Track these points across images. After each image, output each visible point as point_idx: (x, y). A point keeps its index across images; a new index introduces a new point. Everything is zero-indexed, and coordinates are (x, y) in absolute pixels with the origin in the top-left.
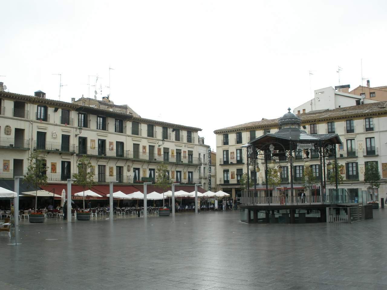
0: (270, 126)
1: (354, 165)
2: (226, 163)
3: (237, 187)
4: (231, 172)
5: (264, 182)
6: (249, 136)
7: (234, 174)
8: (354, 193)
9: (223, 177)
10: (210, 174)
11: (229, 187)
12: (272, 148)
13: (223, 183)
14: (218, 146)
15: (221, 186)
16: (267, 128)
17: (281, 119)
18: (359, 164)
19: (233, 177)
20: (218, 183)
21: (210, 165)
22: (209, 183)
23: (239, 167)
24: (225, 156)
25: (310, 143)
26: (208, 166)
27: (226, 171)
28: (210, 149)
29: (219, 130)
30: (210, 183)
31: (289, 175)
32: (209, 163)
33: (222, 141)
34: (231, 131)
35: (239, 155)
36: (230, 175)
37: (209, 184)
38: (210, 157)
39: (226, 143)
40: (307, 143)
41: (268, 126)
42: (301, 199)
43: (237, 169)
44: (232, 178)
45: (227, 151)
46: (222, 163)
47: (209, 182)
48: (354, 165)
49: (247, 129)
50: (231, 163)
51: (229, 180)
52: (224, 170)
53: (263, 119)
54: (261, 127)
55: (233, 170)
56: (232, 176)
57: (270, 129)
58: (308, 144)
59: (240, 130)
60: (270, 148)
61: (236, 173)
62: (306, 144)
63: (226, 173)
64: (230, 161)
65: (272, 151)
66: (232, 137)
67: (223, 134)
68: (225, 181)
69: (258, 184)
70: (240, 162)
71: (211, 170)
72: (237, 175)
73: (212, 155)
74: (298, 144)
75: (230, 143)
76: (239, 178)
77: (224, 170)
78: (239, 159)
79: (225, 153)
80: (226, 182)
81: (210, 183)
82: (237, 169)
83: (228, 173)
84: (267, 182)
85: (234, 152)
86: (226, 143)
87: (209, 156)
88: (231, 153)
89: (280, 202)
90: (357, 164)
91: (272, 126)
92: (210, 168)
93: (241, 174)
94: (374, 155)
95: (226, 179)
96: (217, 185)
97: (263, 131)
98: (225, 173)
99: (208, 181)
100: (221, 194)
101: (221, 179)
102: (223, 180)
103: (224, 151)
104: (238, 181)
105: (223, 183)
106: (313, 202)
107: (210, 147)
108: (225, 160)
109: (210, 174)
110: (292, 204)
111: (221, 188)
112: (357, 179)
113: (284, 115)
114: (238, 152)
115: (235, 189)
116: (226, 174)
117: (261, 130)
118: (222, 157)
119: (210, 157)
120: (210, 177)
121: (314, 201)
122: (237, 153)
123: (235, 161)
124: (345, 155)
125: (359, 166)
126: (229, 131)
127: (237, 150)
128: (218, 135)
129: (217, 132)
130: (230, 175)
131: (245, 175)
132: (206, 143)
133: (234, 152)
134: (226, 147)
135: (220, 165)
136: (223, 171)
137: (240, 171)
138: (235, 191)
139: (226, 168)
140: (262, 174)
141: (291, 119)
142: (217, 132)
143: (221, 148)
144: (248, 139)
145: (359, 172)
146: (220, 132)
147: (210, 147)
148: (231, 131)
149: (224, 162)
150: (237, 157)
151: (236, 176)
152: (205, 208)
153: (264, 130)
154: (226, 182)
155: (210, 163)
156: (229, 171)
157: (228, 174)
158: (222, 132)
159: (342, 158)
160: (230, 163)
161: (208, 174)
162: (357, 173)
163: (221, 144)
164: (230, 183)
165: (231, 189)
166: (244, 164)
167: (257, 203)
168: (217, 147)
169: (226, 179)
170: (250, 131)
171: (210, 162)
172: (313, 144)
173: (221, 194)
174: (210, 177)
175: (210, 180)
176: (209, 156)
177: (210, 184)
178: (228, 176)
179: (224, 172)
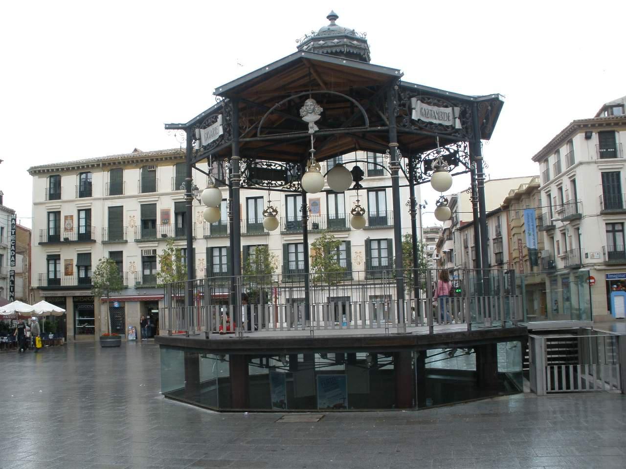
0: (157, 160)
1: (343, 247)
2: (54, 240)
3: (78, 293)
4: (65, 260)
5: (140, 282)
6: (109, 181)
7: (72, 265)
8: (340, 306)
9: (45, 271)
10: (13, 268)
11: (60, 293)
12: (313, 111)
13: (45, 284)
14: (38, 201)
15: (41, 292)
16: (151, 164)
17: (313, 39)
18: (352, 244)
19: (70, 270)
20: (35, 284)
21: (15, 251)
22: (10, 289)
23: (84, 249)
24: (52, 225)
25: (446, 107)
26: (9, 251)
27: (54, 259)
28: (14, 217)
29: (41, 167)
30: (14, 289)
31: (550, 168)
32: (12, 246)
33: (46, 192)
34: (68, 169)
35: (83, 222)
36: (61, 267)
37: (10, 291)
38: (15, 234)
39: (55, 193)
40: (439, 106)
41: (152, 160)
42: (362, 318)
43: (79, 254)
44: (68, 273)
45: (57, 214)
46: (45, 240)
47: (10, 287)
48: (343, 247)
49: (104, 165)
50: (66, 240)
51: (60, 279)
52: (48, 256)
53: (136, 150)
54: (137, 161)
55: (69, 255)
56: (66, 268)
57: (157, 167)
58: (442, 109)
59: (88, 166)
60: (303, 111)
61: (75, 262)
62: (435, 109)
63: (53, 262)
64: (63, 235)
65: (310, 125)
66: (70, 184)
67: (49, 175)
68: (50, 281)
69: (126, 288)
70: (86, 238)
71: (15, 261)
72: (78, 267)
73: (17, 229)
74: (414, 100)
75: (64, 196)
76: (82, 275)
77: (48, 256)
78: (83, 231)
79: (52, 217)
80: (54, 283)
81: (14, 287)
82: (79, 254)
83: (58, 262)
84: (148, 280)
85: (72, 217)
86: (55, 193)
87: (13, 231)
88: (66, 217)
89: (489, 323)
90: (348, 244)
91: (162, 159)
92: (14, 256)
93: (85, 264)
94: (385, 226)
95: (52, 276)
96: (32, 289)
97: (141, 170)
98: (50, 262)
99: (9, 284)
100: (44, 307)
101: (41, 275)
102: (45, 277)
103: (49, 213)
104: (80, 280)
105: (45, 284)
106: (249, 329)
107: (15, 212)
108: (52, 233)
109: (13, 268)
110: (402, 331)
111: (42, 295)
112: (349, 277)
113: (320, 29)
114: (83, 215)
115: (74, 297)
116: (53, 265)
117: (136, 167)
118: (45, 227)
119: (15, 234)
120: (14, 275)
121: (253, 326)
122: (79, 219)
123: (73, 237)
124: (323, 226)
125: (353, 250)
126: (63, 169)
127: (79, 211)
128: (37, 177)
129: (36, 172)
130: (61, 267)
131: (104, 262)
132: (6, 203)
133: (72, 217)
134: (55, 205)
135: (40, 244)
136: (45, 257)
137: (84, 260)
138: (74, 302)
139: (54, 250)
140: (135, 265)
141: (349, 41)
142: (36, 172)
143: (43, 207)
144: (104, 188)
145: (353, 261)
146: (44, 171)
147: (15, 212)
148: (68, 169)
149: (50, 237)
150: (79, 226)
151: (75, 269)
152: (5, 342)
153: (143, 167)
154: (54, 283)
155: (14, 246)
156: (59, 259)
157: (58, 265)
158: (48, 170)
159: (316, 231)
160: (62, 240)
161: (10, 268)
162: (349, 264)
163: (43, 196)
164: (63, 283)
165: (65, 297)
166: (95, 241)
167: (249, 329)
168: (35, 204)
169: (52, 276)
170: (112, 171)
171: (15, 243)
172: (457, 110)
173: (44, 307)
174: (14, 276)
175: (13, 282)
176: (13, 231)
177: (12, 290)
178: (58, 270)
179: (48, 260)
